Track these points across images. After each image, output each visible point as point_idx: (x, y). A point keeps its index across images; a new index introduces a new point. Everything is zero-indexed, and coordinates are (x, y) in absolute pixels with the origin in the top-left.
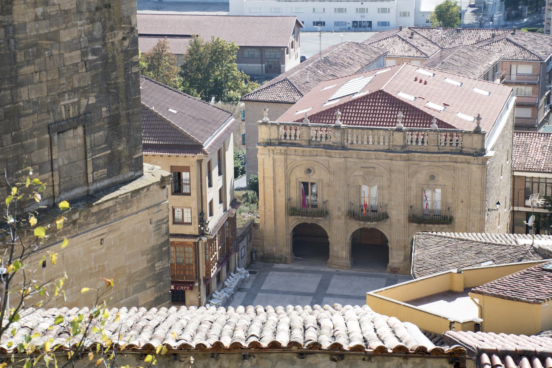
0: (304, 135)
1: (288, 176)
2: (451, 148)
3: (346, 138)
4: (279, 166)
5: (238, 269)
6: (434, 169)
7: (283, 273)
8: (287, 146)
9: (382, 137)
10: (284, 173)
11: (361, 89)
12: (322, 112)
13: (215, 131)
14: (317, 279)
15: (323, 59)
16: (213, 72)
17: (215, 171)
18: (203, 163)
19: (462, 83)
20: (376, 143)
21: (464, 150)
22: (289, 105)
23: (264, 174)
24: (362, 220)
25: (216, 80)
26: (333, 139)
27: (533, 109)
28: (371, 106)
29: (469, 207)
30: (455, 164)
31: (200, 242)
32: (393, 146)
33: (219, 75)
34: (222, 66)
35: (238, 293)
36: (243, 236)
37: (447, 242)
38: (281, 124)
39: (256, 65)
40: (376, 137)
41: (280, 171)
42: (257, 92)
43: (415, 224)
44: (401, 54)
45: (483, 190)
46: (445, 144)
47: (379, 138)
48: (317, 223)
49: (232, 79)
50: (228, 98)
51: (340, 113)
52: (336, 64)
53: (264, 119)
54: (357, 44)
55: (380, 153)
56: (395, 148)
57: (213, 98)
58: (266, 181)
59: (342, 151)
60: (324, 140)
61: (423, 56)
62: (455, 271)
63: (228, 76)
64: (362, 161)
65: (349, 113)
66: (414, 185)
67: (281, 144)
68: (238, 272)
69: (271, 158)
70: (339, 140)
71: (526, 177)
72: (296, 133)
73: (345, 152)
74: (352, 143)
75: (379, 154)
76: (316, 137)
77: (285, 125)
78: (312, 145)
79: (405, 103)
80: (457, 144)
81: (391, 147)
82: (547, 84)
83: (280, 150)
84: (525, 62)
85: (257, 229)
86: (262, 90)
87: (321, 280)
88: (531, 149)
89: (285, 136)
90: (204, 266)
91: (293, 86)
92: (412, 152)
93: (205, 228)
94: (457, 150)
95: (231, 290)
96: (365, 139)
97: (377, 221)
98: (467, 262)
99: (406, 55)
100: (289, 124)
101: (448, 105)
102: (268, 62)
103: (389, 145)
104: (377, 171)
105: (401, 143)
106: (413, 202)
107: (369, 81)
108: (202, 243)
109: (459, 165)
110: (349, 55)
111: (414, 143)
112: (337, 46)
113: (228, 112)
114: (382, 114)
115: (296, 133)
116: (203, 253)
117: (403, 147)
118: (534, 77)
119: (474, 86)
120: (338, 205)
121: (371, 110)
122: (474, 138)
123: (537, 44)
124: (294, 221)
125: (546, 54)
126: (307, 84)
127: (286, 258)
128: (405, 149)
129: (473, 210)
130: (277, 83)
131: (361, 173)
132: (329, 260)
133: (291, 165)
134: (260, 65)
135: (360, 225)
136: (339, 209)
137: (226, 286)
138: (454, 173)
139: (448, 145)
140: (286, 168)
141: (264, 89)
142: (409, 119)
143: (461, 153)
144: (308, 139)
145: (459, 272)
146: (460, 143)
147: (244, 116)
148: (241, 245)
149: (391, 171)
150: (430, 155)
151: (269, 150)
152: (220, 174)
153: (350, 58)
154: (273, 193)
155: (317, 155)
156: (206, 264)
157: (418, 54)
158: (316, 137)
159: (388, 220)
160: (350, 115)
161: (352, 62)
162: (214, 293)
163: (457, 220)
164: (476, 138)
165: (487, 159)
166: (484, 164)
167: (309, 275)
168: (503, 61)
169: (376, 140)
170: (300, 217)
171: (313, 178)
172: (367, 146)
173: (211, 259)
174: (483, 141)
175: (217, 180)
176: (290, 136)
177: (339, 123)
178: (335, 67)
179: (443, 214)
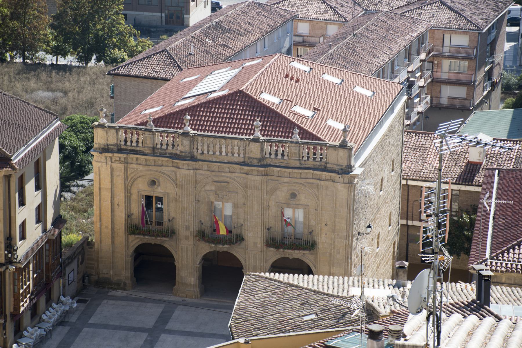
0: (148, 142)
1: (129, 188)
2: (314, 163)
3: (195, 147)
4: (118, 176)
5: (62, 298)
6: (295, 186)
7: (119, 302)
8: (127, 154)
9: (236, 148)
10: (123, 185)
11: (221, 85)
12: (171, 114)
13: (31, 139)
14: (156, 310)
15: (214, 23)
16: (94, 25)
17: (30, 186)
18: (12, 179)
19: (343, 81)
20: (230, 155)
21: (328, 166)
22: (164, 81)
23: (100, 185)
24: (213, 242)
25: (96, 36)
26: (181, 148)
27: (468, 88)
28: (229, 109)
29: (334, 231)
30: (318, 181)
31: (7, 271)
32: (249, 158)
33: (101, 29)
34: (105, 19)
35: (60, 328)
36: (71, 259)
37: (276, 286)
38: (120, 127)
39: (155, 14)
40: (230, 147)
41: (120, 183)
42: (129, 64)
43: (272, 249)
44: (315, 16)
45: (350, 213)
46: (308, 158)
47: (233, 149)
48: (162, 244)
49: (117, 35)
50: (111, 58)
51: (189, 117)
52: (230, 31)
53: (100, 121)
54: (260, 4)
55: (234, 166)
56: (251, 160)
57: (94, 57)
58: (103, 193)
59: (190, 162)
60: (170, 148)
61: (341, 19)
62: (242, 340)
63: (113, 31)
64: (214, 174)
65: (202, 116)
66: (272, 203)
67: (120, 151)
68: (62, 302)
69: (109, 166)
70: (187, 149)
71: (422, 187)
72: (138, 138)
73: (194, 163)
74: (203, 153)
75: (233, 168)
76: (162, 144)
77: (126, 129)
78: (156, 153)
79: (267, 106)
80: (321, 158)
81: (247, 160)
82: (487, 57)
83: (120, 158)
84: (460, 31)
85: (91, 248)
86: (135, 62)
87: (163, 312)
88: (430, 153)
89: (126, 141)
90: (12, 299)
91: (173, 59)
92: (270, 166)
93: (13, 255)
94: (321, 165)
95: (47, 326)
96: (218, 149)
97: (229, 244)
98: (290, 314)
99: (322, 18)
100: (130, 128)
101: (319, 110)
102: (169, 10)
103: (244, 157)
104: (231, 186)
105: (258, 156)
106: (272, 223)
107: (233, 74)
108: (10, 273)
109: (322, 183)
110: (248, 20)
111: (273, 156)
112: (235, 6)
113: (52, 114)
114: (240, 119)
115: (138, 138)
116: (10, 284)
117: (260, 160)
118: (471, 50)
119: (356, 84)
120: (187, 224)
121: (227, 114)
122: (340, 153)
123: (477, 8)
124: (136, 241)
125: (486, 22)
126: (189, 57)
127: (125, 284)
128: (262, 163)
129: (338, 235)
130: (154, 55)
131: (213, 188)
132: (175, 287)
133: (132, 175)
134: (159, 14)
135: (211, 247)
136: (187, 228)
137: (43, 321)
138: (318, 191)
139: (311, 159)
140: (126, 178)
141: (138, 61)
142: (269, 127)
143: (325, 169)
144: (152, 146)
145: (246, 342)
146: (324, 158)
147: (113, 93)
148: (68, 270)
149: (246, 187)
150: (290, 170)
151: (106, 157)
152: (37, 188)
153: (249, 23)
154: (110, 207)
155: (163, 165)
156: (14, 297)
157: (336, 18)
158: (162, 144)
159: (243, 243)
160: (203, 118)
161: (250, 28)
162: (26, 330)
163: (320, 246)
164: (342, 153)
165: (354, 177)
166: (350, 182)
167: (149, 305)
168: (432, 30)
169: (230, 150)
170: (142, 237)
171: (157, 192)
172: (220, 157)
173: (21, 291)
174: (350, 157)
175: (33, 197)
176: (132, 142)
177: (188, 129)
178: (228, 35)
179: (305, 238)
